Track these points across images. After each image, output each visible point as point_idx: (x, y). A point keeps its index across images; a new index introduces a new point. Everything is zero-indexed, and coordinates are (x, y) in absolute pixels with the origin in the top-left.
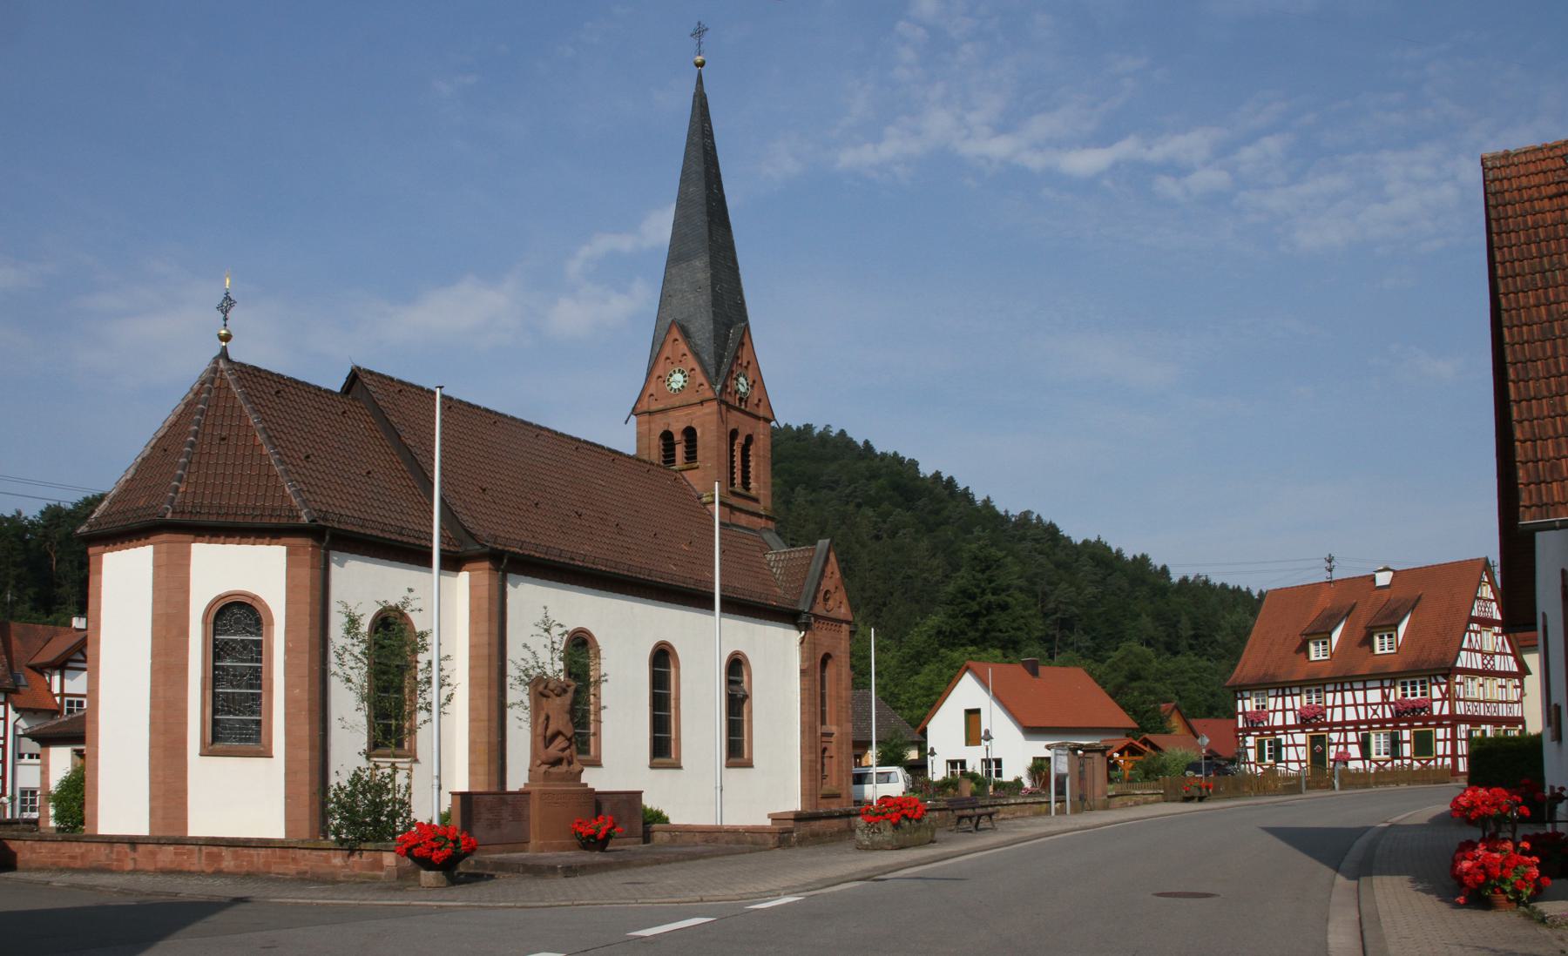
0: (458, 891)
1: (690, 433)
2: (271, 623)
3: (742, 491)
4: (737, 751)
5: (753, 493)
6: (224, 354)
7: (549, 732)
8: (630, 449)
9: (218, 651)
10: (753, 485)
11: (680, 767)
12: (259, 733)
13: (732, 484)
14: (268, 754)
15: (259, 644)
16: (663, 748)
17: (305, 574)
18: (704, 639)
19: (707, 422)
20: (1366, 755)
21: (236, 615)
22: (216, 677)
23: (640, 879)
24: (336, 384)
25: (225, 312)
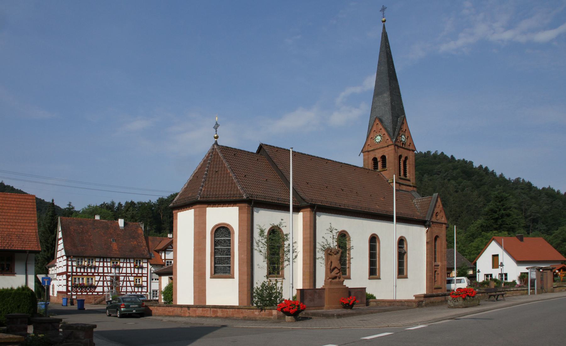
0: (299, 323)
1: (383, 158)
2: (234, 233)
3: (404, 178)
4: (401, 272)
5: (408, 178)
6: (216, 143)
7: (332, 268)
9: (216, 243)
10: (408, 175)
12: (230, 270)
13: (400, 175)
14: (233, 277)
15: (229, 240)
16: (373, 272)
17: (245, 216)
18: (389, 232)
19: (390, 153)
21: (222, 231)
25: (216, 129)
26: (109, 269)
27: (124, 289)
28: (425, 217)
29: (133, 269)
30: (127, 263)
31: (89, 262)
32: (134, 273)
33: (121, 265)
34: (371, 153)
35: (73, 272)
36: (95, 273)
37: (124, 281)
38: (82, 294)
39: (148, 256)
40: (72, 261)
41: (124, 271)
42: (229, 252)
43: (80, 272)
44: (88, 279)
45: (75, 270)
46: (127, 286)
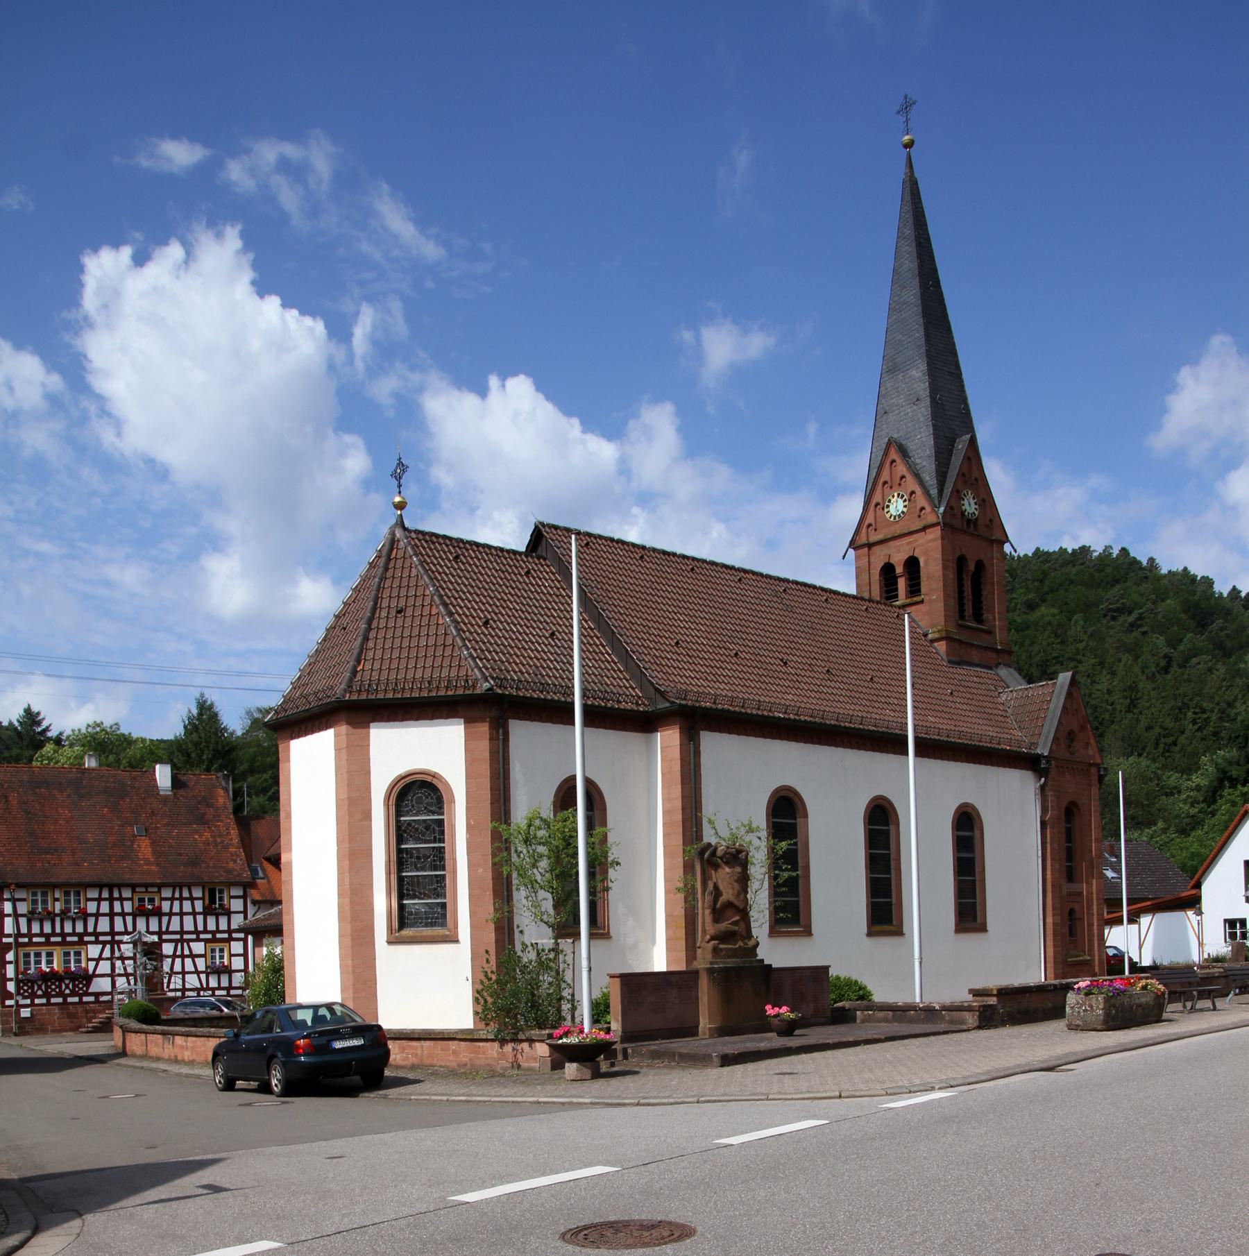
0: (600, 1084)
1: (912, 565)
2: (452, 800)
4: (969, 914)
6: (401, 523)
8: (852, 590)
9: (401, 832)
11: (457, 941)
12: (444, 916)
14: (454, 940)
15: (440, 823)
16: (884, 914)
17: (484, 746)
18: (923, 794)
19: (930, 550)
20: (50, 962)
21: (418, 794)
22: (401, 860)
23: (798, 1068)
24: (517, 540)
25: (398, 478)
26: (129, 919)
27: (176, 982)
28: (1035, 745)
29: (200, 918)
30: (181, 899)
31: (67, 902)
32: (205, 931)
33: (92, 907)
34: (876, 549)
35: (19, 935)
36: (86, 933)
37: (174, 956)
38: (49, 1003)
39: (247, 875)
40: (14, 901)
41: (175, 925)
42: (439, 859)
43: (74, 934)
44: (67, 954)
45: (24, 930)
46: (184, 973)
